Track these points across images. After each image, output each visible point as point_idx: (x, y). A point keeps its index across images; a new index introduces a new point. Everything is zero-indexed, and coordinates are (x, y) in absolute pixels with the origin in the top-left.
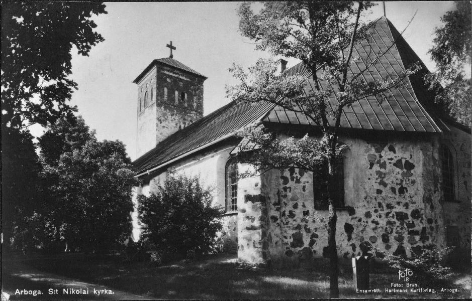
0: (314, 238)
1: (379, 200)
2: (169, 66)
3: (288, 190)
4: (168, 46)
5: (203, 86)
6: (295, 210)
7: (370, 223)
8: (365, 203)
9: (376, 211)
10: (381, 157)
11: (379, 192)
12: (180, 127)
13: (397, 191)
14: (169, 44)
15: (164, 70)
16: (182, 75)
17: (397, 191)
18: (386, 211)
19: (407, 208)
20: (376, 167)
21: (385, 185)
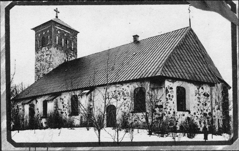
1: (198, 108)
2: (59, 24)
4: (55, 10)
5: (77, 37)
7: (195, 117)
8: (194, 109)
9: (197, 112)
10: (199, 91)
11: (198, 105)
12: (65, 60)
13: (204, 105)
15: (56, 26)
16: (66, 30)
17: (204, 105)
18: (201, 112)
19: (207, 111)
20: (197, 95)
21: (200, 102)
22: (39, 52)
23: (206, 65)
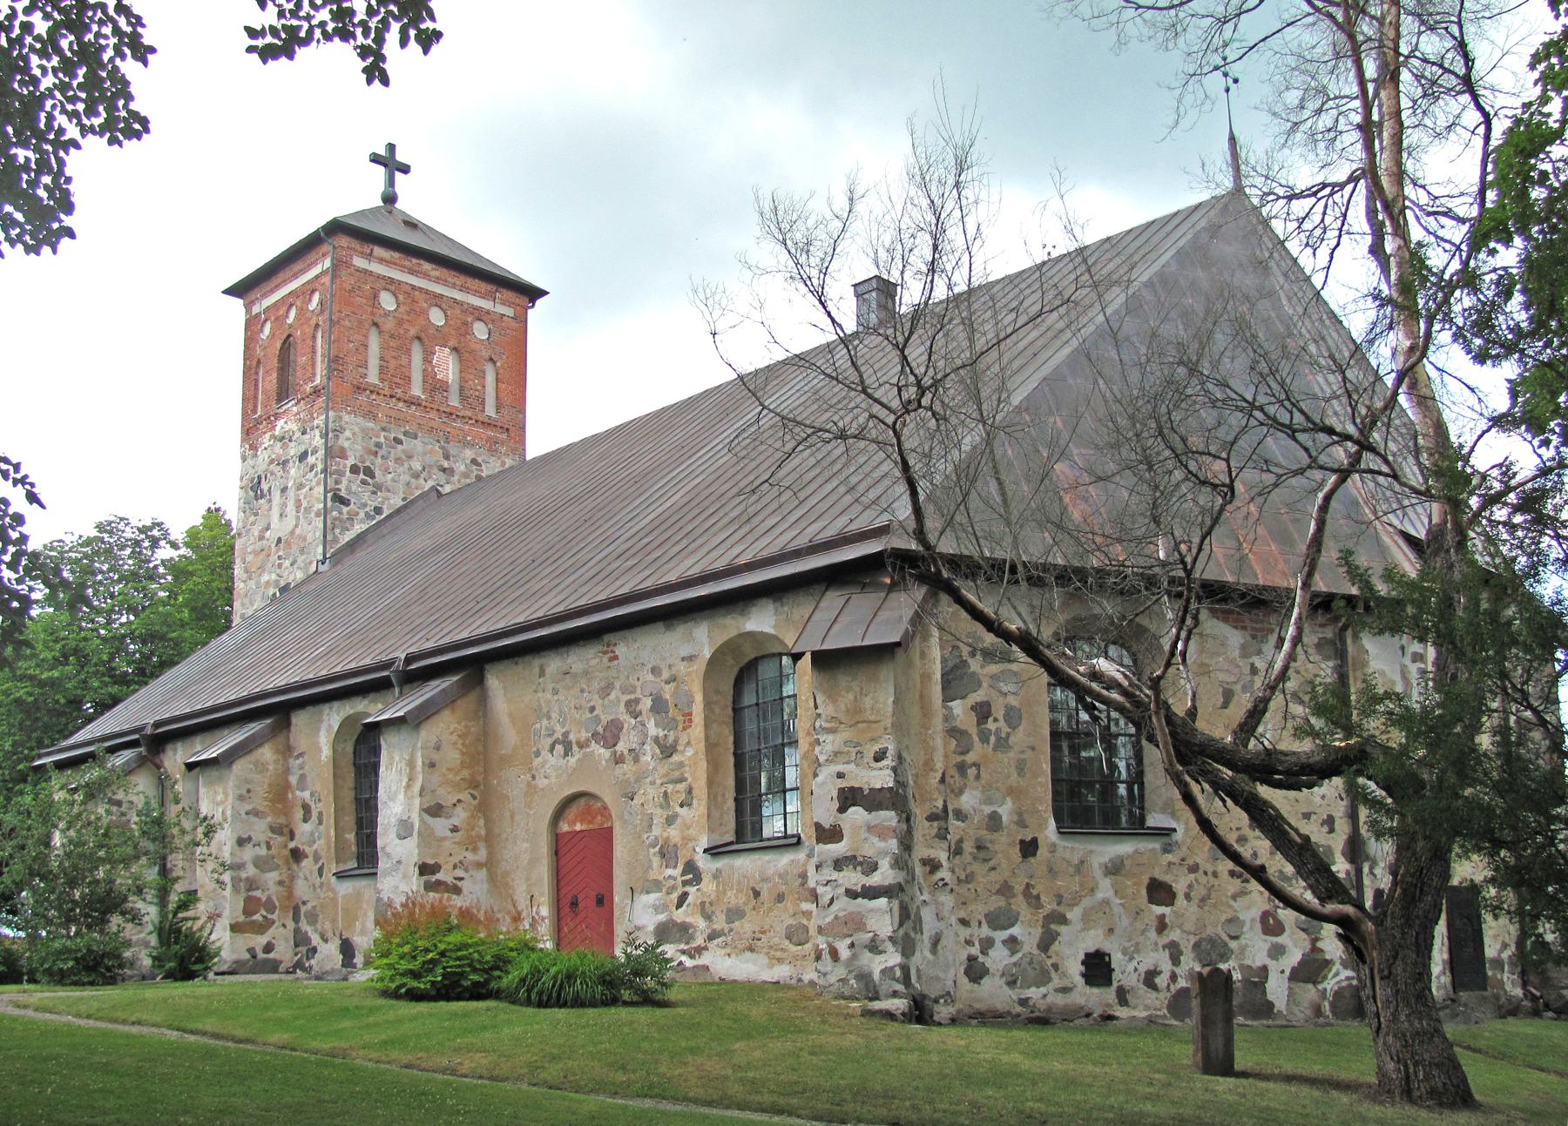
0: (1053, 926)
3: (972, 772)
6: (1267, 907)
14: (382, 152)
22: (266, 440)
23: (1180, 646)
